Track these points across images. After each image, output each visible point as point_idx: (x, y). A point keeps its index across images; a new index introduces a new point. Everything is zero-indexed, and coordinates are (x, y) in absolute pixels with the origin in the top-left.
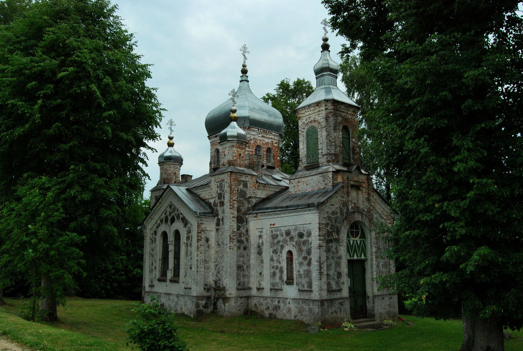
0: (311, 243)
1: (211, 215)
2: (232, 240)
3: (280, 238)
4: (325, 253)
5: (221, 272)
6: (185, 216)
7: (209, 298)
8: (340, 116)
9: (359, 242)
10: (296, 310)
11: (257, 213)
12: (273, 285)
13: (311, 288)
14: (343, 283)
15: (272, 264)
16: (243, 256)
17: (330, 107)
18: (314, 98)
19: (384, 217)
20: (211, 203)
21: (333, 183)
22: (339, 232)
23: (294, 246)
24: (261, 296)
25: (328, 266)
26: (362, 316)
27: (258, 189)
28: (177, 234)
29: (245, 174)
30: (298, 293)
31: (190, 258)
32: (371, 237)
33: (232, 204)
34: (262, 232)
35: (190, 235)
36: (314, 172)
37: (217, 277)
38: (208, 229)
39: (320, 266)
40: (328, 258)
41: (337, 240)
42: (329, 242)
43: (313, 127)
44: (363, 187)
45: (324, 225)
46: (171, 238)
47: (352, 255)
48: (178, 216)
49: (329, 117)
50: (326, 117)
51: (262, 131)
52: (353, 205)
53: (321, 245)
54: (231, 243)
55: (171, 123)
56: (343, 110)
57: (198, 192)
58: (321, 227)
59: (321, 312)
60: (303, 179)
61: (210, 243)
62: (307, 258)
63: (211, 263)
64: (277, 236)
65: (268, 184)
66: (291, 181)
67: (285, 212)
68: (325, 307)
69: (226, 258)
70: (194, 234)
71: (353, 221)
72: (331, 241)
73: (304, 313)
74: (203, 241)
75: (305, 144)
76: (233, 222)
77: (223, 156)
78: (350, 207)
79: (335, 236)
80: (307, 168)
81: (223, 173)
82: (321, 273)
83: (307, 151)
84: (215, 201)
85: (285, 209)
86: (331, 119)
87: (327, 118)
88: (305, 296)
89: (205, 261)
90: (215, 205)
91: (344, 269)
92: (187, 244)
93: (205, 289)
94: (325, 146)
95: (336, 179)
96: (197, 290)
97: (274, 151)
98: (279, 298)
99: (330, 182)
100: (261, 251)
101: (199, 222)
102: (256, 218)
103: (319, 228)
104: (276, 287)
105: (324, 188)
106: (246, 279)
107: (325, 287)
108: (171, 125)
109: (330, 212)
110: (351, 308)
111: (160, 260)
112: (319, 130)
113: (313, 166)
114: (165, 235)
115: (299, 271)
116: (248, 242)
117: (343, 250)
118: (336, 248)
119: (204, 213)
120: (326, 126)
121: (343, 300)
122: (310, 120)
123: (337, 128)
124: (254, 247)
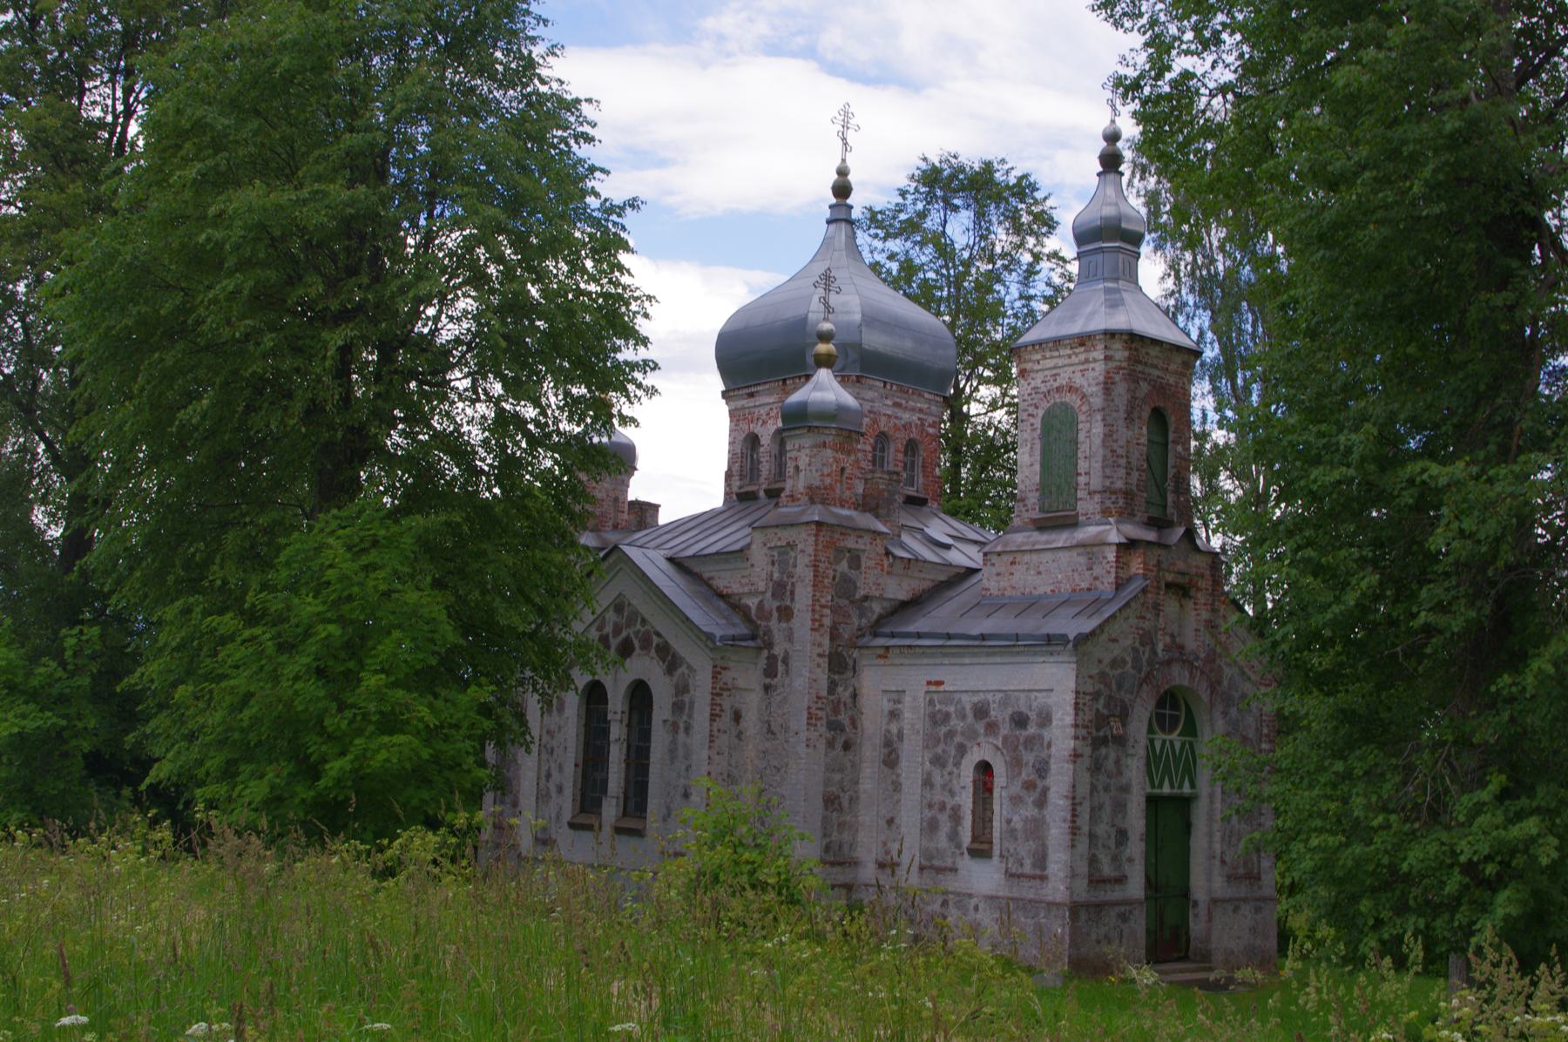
0: (1049, 745)
1: (750, 643)
2: (813, 721)
4: (1087, 775)
6: (671, 642)
8: (1145, 380)
9: (1177, 746)
11: (887, 648)
12: (928, 854)
13: (1044, 868)
14: (1130, 860)
16: (841, 770)
17: (1120, 353)
18: (1072, 319)
19: (1253, 677)
20: (748, 607)
21: (1117, 577)
22: (1127, 715)
23: (998, 748)
25: (1092, 809)
26: (1176, 955)
27: (888, 573)
28: (640, 694)
29: (855, 529)
30: (1003, 882)
31: (683, 767)
32: (1212, 734)
33: (817, 616)
34: (899, 702)
35: (686, 698)
36: (1062, 538)
38: (741, 683)
39: (1074, 810)
40: (1093, 788)
41: (1120, 741)
42: (1098, 743)
43: (1066, 407)
44: (1199, 589)
45: (1088, 697)
46: (617, 703)
47: (1157, 783)
49: (1113, 383)
50: (1106, 383)
51: (894, 388)
52: (1168, 639)
53: (1079, 751)
56: (1155, 361)
57: (707, 571)
58: (1081, 701)
59: (1071, 935)
60: (1027, 558)
61: (743, 724)
63: (744, 785)
64: (947, 716)
65: (917, 560)
71: (1167, 687)
72: (1104, 741)
74: (727, 718)
75: (1037, 452)
78: (1160, 646)
79: (1116, 727)
80: (1041, 526)
81: (792, 525)
82: (1074, 831)
84: (761, 602)
85: (976, 643)
86: (1121, 389)
87: (1108, 386)
88: (1027, 891)
89: (729, 776)
91: (1136, 821)
94: (1097, 465)
95: (1127, 564)
97: (925, 450)
98: (946, 893)
99: (1109, 572)
100: (893, 756)
101: (717, 663)
102: (882, 661)
103: (1076, 704)
104: (936, 863)
105: (1089, 589)
106: (846, 836)
107: (1083, 868)
109: (1106, 661)
110: (1148, 932)
111: (576, 765)
112: (1082, 418)
113: (1057, 520)
116: (855, 728)
117: (1135, 769)
118: (1117, 762)
119: (734, 638)
120: (1104, 409)
121: (1128, 908)
122: (1056, 384)
123: (1136, 414)
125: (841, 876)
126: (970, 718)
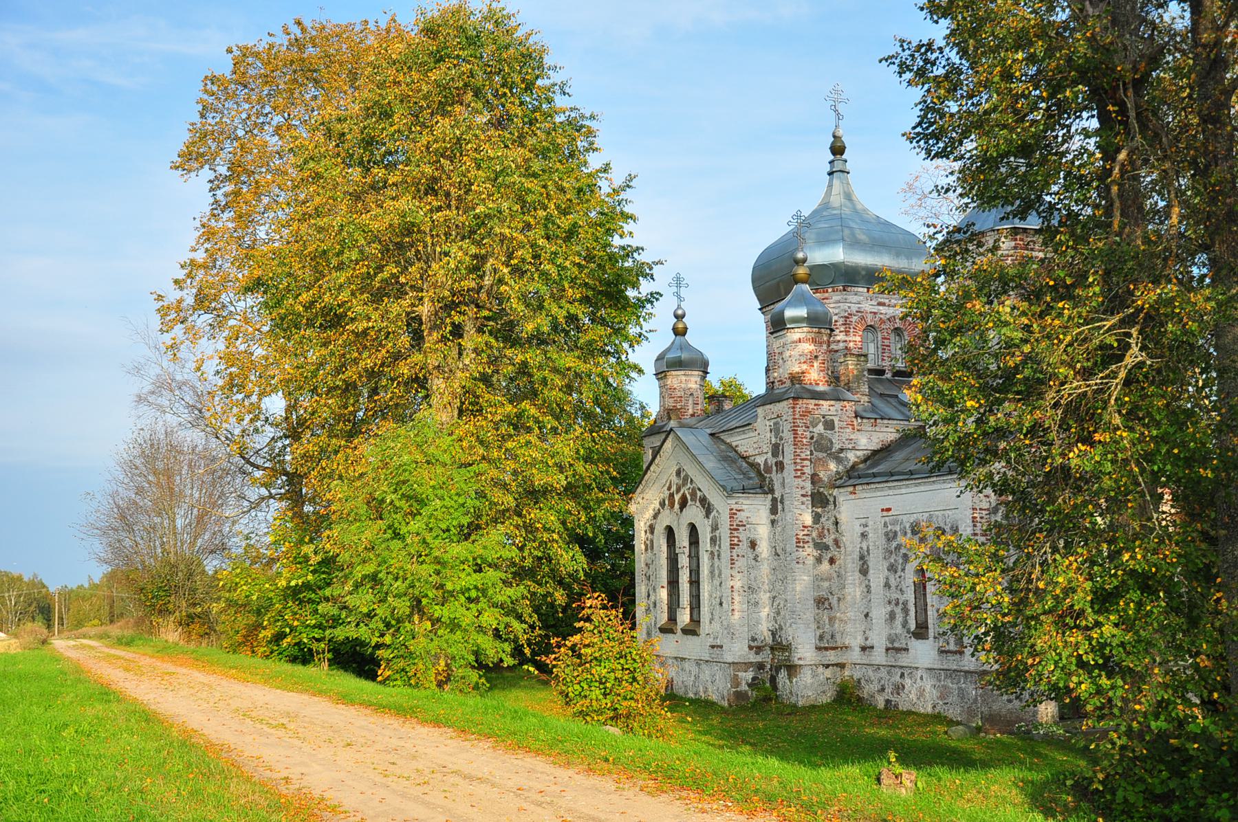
2: (801, 544)
3: (901, 539)
5: (782, 613)
7: (760, 666)
11: (855, 486)
24: (868, 662)
28: (693, 529)
30: (937, 658)
33: (799, 467)
35: (717, 533)
38: (753, 520)
45: (984, 512)
46: (683, 540)
48: (693, 494)
55: (678, 281)
61: (758, 549)
67: (907, 482)
70: (724, 532)
74: (745, 545)
76: (803, 507)
77: (781, 361)
89: (749, 588)
90: (768, 469)
92: (712, 553)
93: (751, 648)
96: (738, 650)
98: (902, 667)
101: (733, 506)
102: (853, 496)
104: (896, 645)
108: (679, 286)
114: (670, 532)
124: (853, 559)
125: (832, 657)
126: (909, 535)
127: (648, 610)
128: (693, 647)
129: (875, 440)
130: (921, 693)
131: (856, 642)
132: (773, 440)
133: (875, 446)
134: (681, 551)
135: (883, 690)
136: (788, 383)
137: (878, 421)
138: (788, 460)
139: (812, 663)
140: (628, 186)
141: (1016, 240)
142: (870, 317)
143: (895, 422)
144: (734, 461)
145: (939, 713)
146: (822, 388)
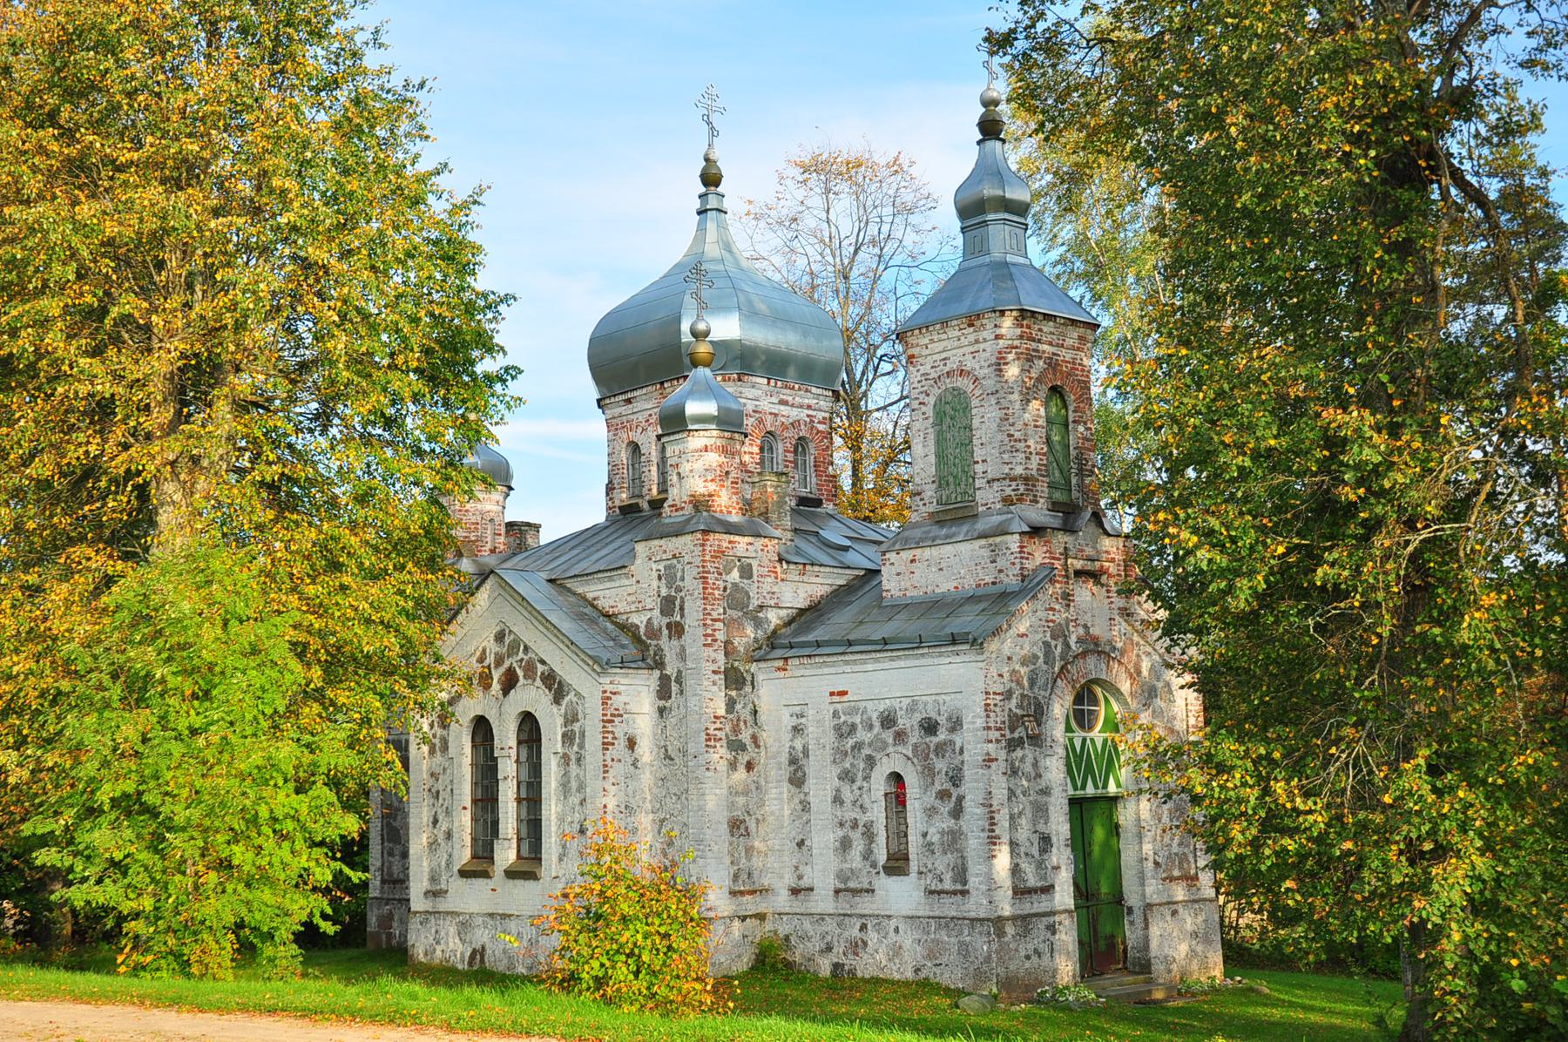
0: (962, 751)
2: (712, 743)
3: (862, 735)
4: (1004, 778)
5: (677, 843)
10: (918, 949)
11: (786, 659)
12: (842, 876)
15: (839, 814)
20: (637, 627)
24: (803, 911)
25: (1012, 817)
28: (529, 727)
31: (577, 801)
33: (709, 631)
35: (576, 727)
37: (665, 855)
38: (633, 707)
41: (1036, 740)
43: (958, 393)
46: (506, 737)
47: (1079, 785)
48: (530, 670)
52: (1081, 631)
53: (993, 756)
54: (712, 750)
61: (639, 750)
62: (950, 796)
64: (853, 727)
66: (888, 556)
67: (878, 655)
68: (1006, 939)
69: (695, 797)
72: (1019, 743)
73: (944, 960)
74: (621, 744)
78: (1073, 640)
83: (938, 465)
84: (650, 619)
88: (949, 907)
89: (626, 807)
90: (653, 633)
91: (1060, 826)
92: (566, 757)
99: (1014, 564)
100: (800, 774)
102: (782, 674)
104: (852, 885)
105: (994, 583)
110: (1081, 943)
112: (975, 402)
114: (482, 728)
115: (925, 835)
117: (1054, 770)
118: (1035, 764)
122: (947, 369)
124: (780, 764)
125: (751, 904)
126: (877, 728)
127: (433, 845)
128: (523, 897)
129: (802, 595)
130: (897, 951)
131: (781, 882)
132: (664, 592)
133: (802, 603)
134: (504, 753)
135: (829, 949)
136: (689, 510)
137: (808, 567)
138: (692, 619)
139: (726, 914)
140: (475, 202)
141: (1022, 326)
142: (769, 419)
143: (828, 569)
144: (593, 622)
145: (926, 979)
146: (735, 518)
